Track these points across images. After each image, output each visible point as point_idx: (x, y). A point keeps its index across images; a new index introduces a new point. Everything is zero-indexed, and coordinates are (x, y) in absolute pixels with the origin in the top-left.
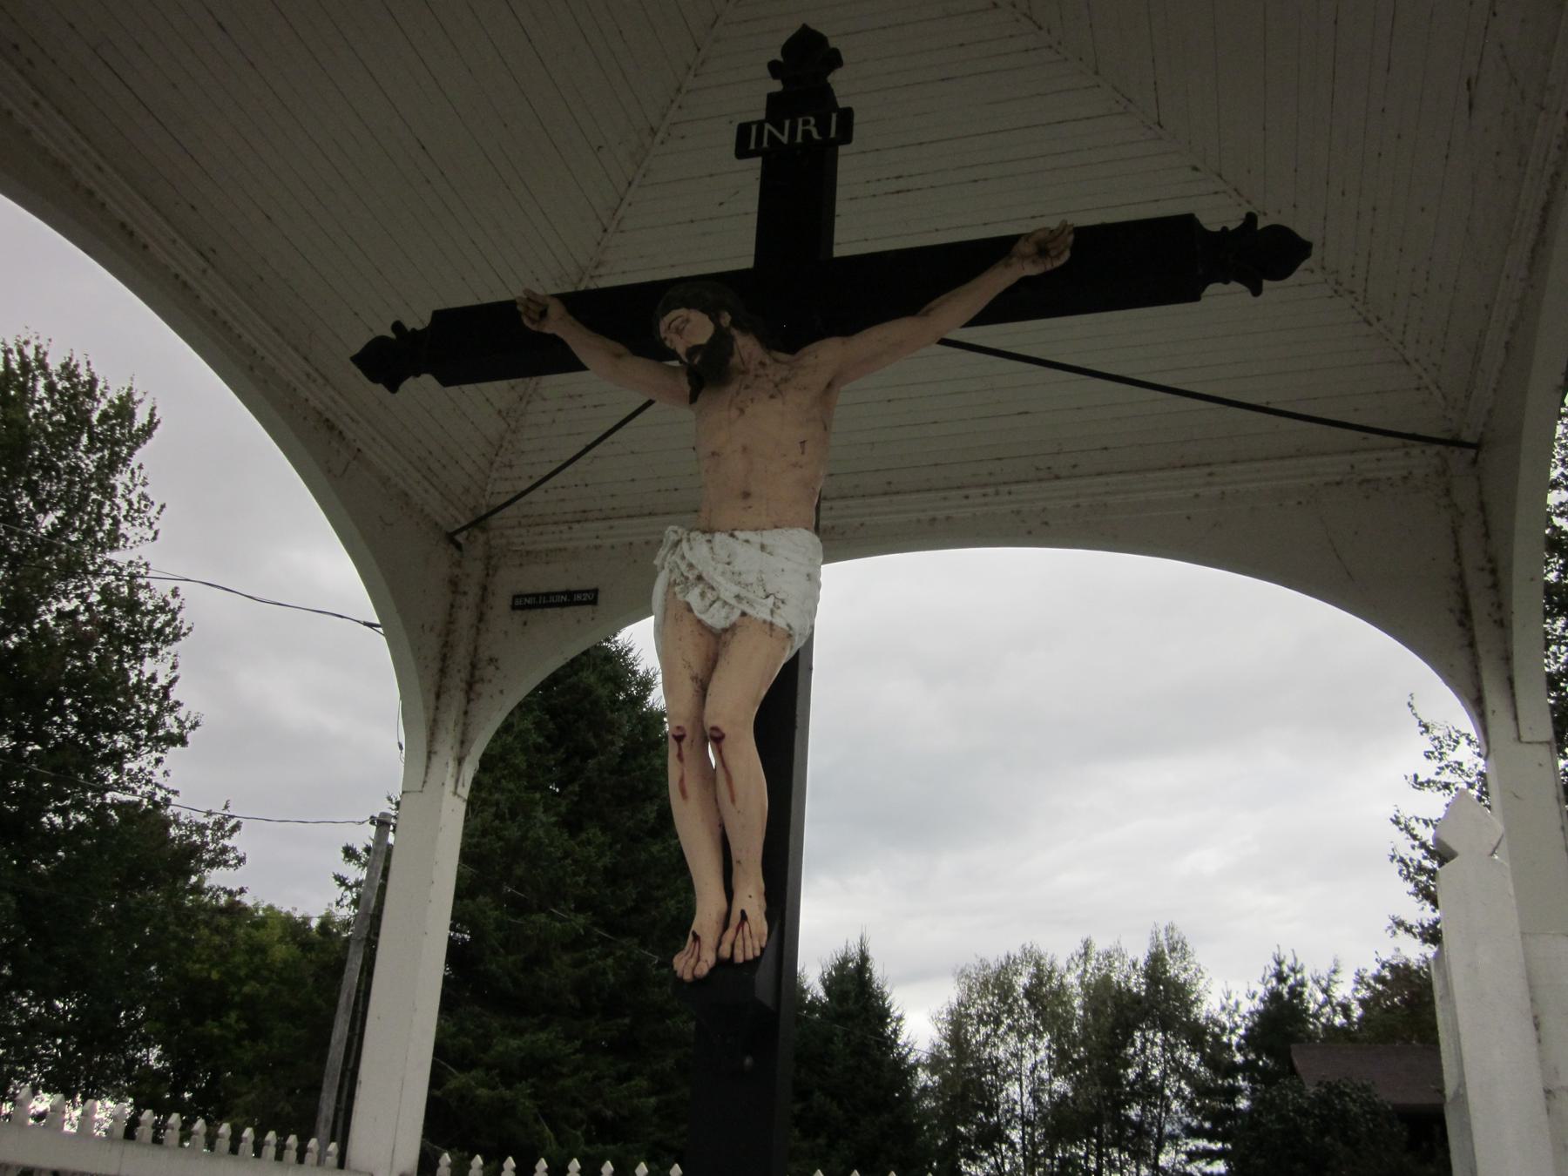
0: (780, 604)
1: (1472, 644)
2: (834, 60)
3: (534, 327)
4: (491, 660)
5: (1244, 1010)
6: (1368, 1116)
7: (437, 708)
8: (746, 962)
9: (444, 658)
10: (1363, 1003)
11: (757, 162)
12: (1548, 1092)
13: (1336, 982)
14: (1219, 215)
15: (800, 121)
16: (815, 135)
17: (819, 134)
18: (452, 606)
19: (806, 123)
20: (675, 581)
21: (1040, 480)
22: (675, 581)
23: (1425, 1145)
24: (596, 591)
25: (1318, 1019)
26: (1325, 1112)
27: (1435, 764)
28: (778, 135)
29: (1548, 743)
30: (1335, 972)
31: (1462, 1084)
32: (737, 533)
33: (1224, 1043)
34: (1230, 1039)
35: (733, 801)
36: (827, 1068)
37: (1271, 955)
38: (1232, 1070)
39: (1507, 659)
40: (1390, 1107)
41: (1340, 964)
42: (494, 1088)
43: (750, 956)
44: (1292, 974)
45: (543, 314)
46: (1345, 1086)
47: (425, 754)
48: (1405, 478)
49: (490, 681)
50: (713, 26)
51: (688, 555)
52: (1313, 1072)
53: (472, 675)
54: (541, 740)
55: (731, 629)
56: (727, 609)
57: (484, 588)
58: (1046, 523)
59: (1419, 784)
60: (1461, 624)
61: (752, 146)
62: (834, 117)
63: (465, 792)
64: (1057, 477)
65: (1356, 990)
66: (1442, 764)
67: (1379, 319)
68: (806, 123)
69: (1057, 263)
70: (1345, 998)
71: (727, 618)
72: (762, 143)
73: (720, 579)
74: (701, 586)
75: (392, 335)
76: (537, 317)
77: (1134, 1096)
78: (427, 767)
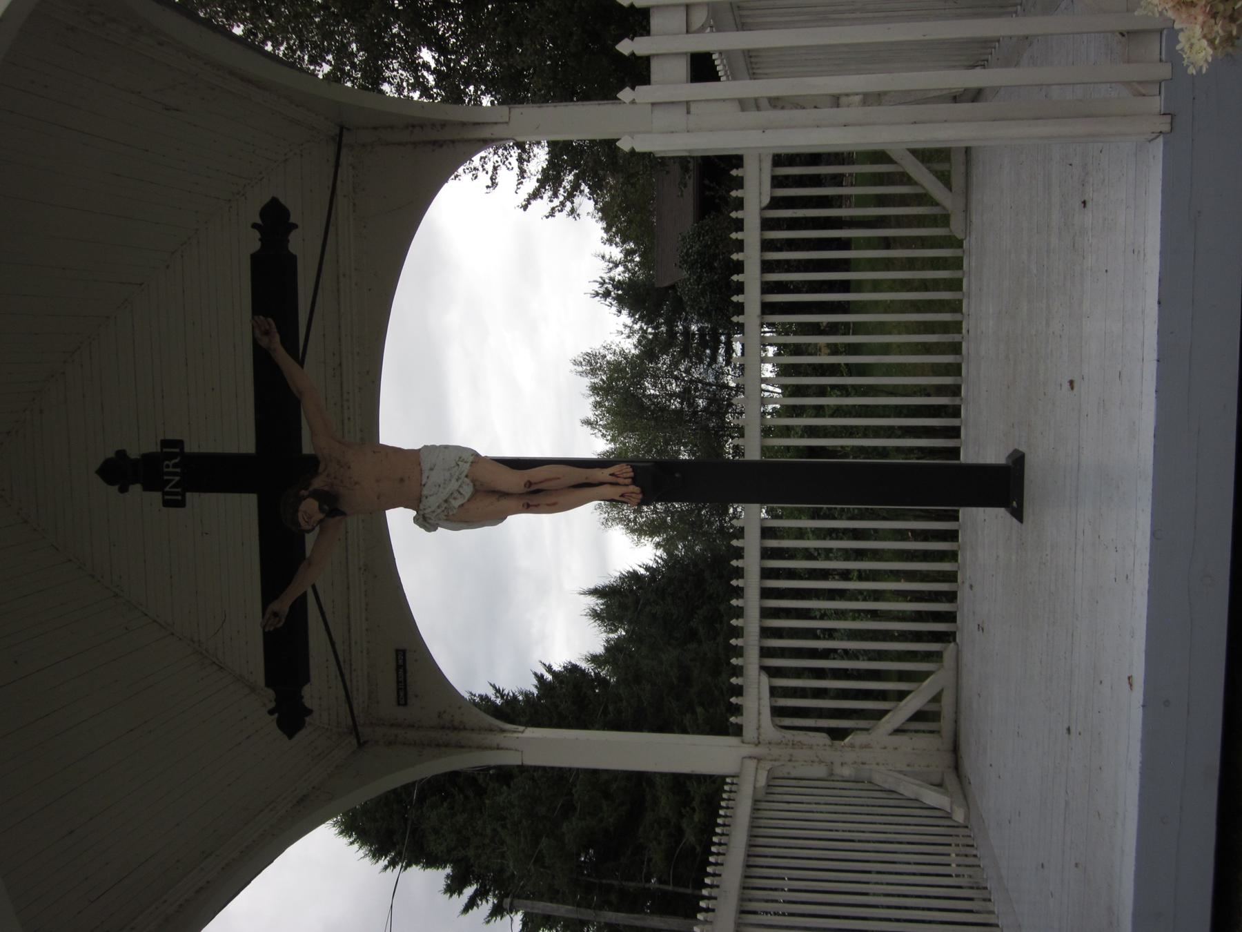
0: (461, 459)
1: (453, 142)
2: (121, 454)
3: (283, 620)
4: (439, 717)
5: (629, 321)
6: (701, 238)
7: (470, 747)
8: (633, 471)
9: (438, 745)
10: (624, 242)
11: (188, 495)
12: (688, 131)
13: (611, 257)
14: (254, 242)
15: (166, 470)
16: (177, 461)
17: (176, 458)
18: (404, 744)
19: (168, 466)
20: (446, 516)
21: (341, 375)
22: (446, 516)
23: (717, 201)
24: (397, 651)
25: (636, 272)
26: (699, 265)
27: (481, 174)
28: (173, 482)
29: (510, 109)
30: (603, 257)
31: (686, 150)
32: (423, 483)
33: (653, 338)
34: (650, 334)
35: (559, 478)
36: (674, 617)
37: (592, 299)
38: (671, 333)
39: (463, 124)
40: (696, 225)
41: (598, 253)
42: (694, 810)
43: (631, 470)
44: (606, 286)
45: (275, 614)
46: (682, 252)
47: (499, 751)
48: (354, 168)
49: (453, 716)
50: (57, 549)
51: (433, 509)
52: (675, 273)
53: (449, 728)
54: (445, 805)
55: (473, 481)
56: (464, 486)
57: (392, 725)
58: (368, 372)
59: (494, 184)
60: (441, 146)
61: (179, 498)
62: (165, 450)
63: (521, 728)
64: (340, 364)
65: (616, 244)
66: (481, 169)
67: (261, 173)
68: (168, 466)
69: (273, 325)
70: (621, 252)
71: (468, 485)
72: (178, 492)
73: (448, 490)
74: (451, 500)
75: (276, 715)
76: (278, 618)
77: (692, 404)
78: (507, 749)
